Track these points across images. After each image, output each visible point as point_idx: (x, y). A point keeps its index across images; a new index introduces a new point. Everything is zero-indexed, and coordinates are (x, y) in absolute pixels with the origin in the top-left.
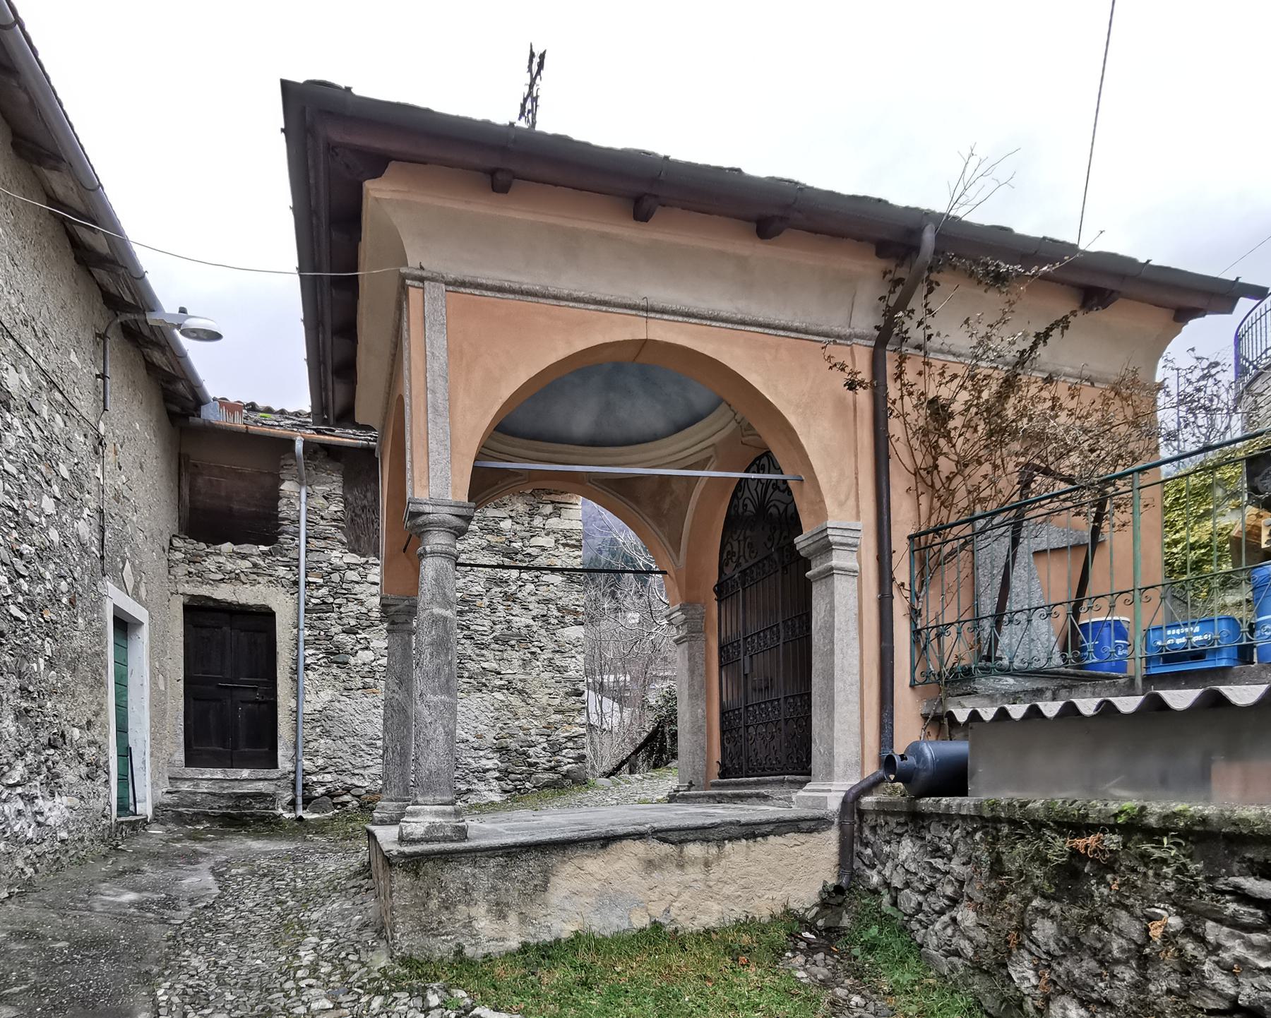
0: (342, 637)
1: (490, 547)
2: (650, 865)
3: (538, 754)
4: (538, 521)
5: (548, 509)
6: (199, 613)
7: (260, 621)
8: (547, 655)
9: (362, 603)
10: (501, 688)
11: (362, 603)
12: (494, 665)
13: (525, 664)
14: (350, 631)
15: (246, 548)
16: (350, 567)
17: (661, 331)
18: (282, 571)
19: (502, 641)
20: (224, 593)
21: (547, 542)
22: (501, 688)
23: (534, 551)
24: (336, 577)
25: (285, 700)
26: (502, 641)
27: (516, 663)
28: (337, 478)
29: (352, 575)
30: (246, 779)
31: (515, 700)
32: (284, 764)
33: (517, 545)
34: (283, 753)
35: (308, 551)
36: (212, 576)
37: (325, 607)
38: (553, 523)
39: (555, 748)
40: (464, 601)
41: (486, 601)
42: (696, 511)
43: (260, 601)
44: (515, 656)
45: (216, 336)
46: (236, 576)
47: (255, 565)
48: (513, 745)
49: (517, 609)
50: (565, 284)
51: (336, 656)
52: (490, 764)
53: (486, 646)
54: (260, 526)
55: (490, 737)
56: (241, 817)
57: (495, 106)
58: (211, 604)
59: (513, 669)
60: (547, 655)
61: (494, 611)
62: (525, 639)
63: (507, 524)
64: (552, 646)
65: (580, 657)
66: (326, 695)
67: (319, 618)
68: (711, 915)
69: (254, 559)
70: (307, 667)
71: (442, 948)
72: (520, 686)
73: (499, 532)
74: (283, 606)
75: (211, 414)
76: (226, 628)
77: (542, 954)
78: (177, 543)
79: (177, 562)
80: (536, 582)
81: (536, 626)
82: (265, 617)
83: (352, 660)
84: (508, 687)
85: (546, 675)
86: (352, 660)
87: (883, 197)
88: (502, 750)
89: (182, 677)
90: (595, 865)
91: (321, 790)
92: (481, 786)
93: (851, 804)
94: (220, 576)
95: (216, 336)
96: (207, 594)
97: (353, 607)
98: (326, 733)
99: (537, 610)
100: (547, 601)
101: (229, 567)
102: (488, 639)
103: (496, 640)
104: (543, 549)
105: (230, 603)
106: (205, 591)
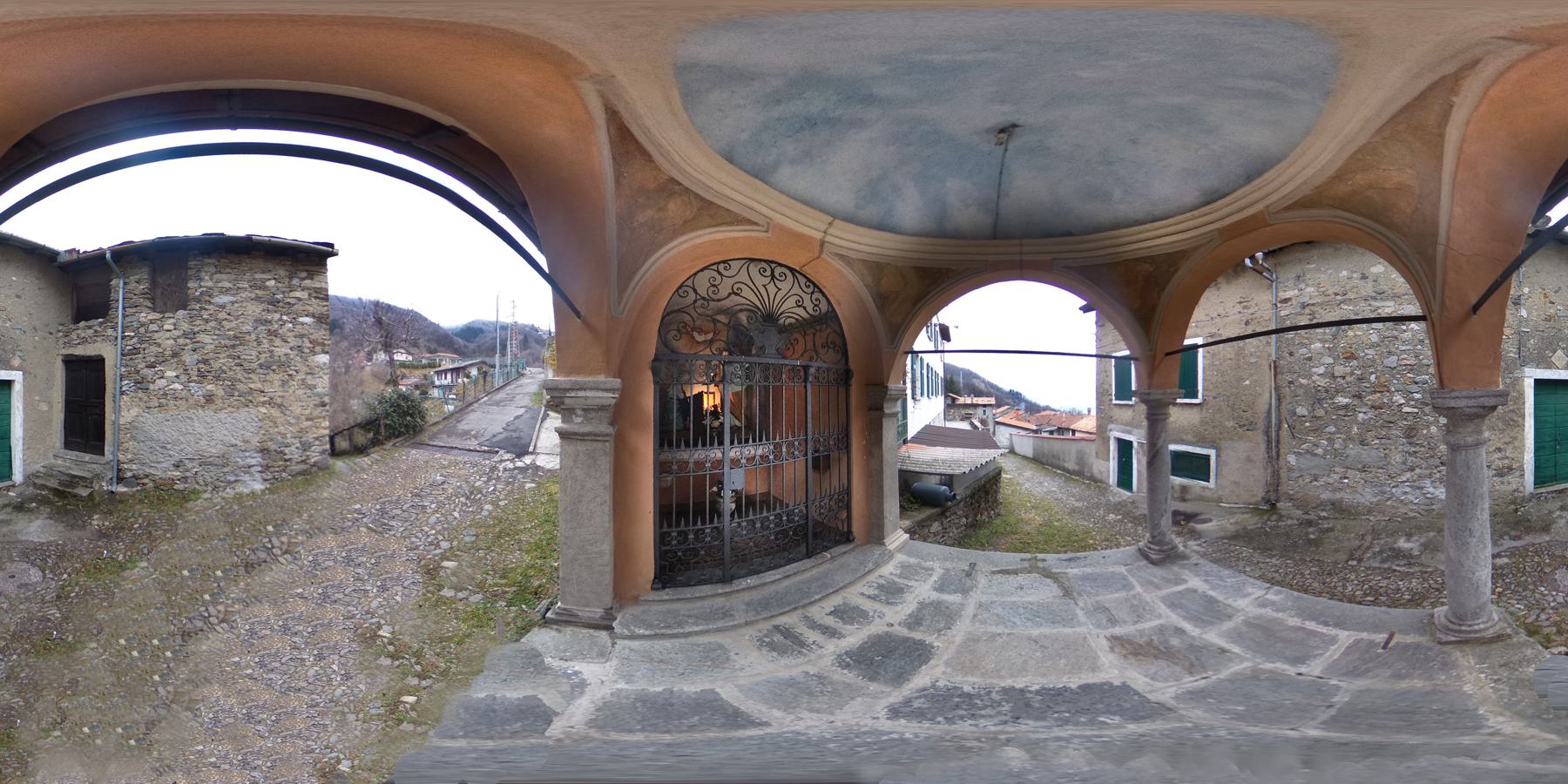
0: (146, 371)
1: (258, 298)
3: (293, 452)
4: (295, 282)
5: (304, 275)
6: (71, 363)
7: (99, 362)
8: (301, 376)
9: (159, 345)
10: (264, 403)
11: (159, 345)
12: (259, 386)
13: (284, 383)
14: (151, 366)
15: (91, 323)
16: (152, 322)
18: (110, 332)
19: (266, 366)
21: (303, 295)
22: (264, 403)
23: (292, 301)
24: (142, 330)
25: (109, 416)
26: (266, 366)
27: (277, 383)
28: (145, 270)
29: (153, 327)
31: (275, 412)
32: (108, 455)
33: (279, 296)
34: (108, 448)
35: (124, 316)
37: (135, 351)
38: (308, 282)
39: (306, 447)
40: (236, 337)
41: (253, 336)
44: (276, 378)
48: (273, 446)
49: (278, 342)
51: (141, 384)
52: (254, 462)
53: (254, 371)
55: (255, 442)
59: (274, 389)
60: (301, 376)
61: (259, 343)
62: (283, 365)
63: (272, 283)
64: (305, 369)
65: (326, 378)
66: (134, 412)
70: (122, 393)
72: (279, 401)
73: (265, 288)
74: (110, 353)
80: (294, 321)
81: (292, 354)
82: (99, 362)
83: (152, 387)
84: (270, 402)
85: (300, 392)
86: (152, 387)
87: (400, 299)
88: (264, 451)
91: (129, 474)
92: (246, 478)
97: (154, 349)
98: (133, 438)
99: (293, 342)
100: (302, 336)
102: (254, 366)
103: (261, 366)
104: (299, 299)
106: (70, 351)
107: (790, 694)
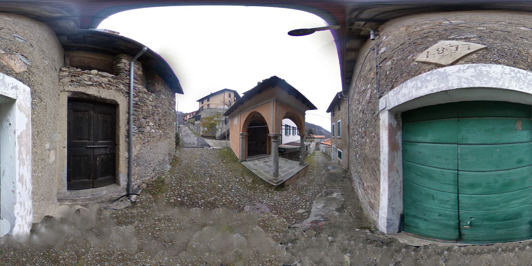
6: (77, 102)
15: (105, 74)
18: (121, 87)
20: (92, 91)
36: (86, 82)
42: (377, 146)
43: (112, 98)
45: (293, 33)
47: (109, 81)
58: (85, 96)
67: (21, 180)
69: (109, 79)
76: (92, 112)
78: (64, 69)
79: (64, 77)
89: (66, 146)
94: (90, 83)
95: (293, 33)
96: (83, 91)
101: (95, 79)
105: (96, 97)
107: (260, 163)
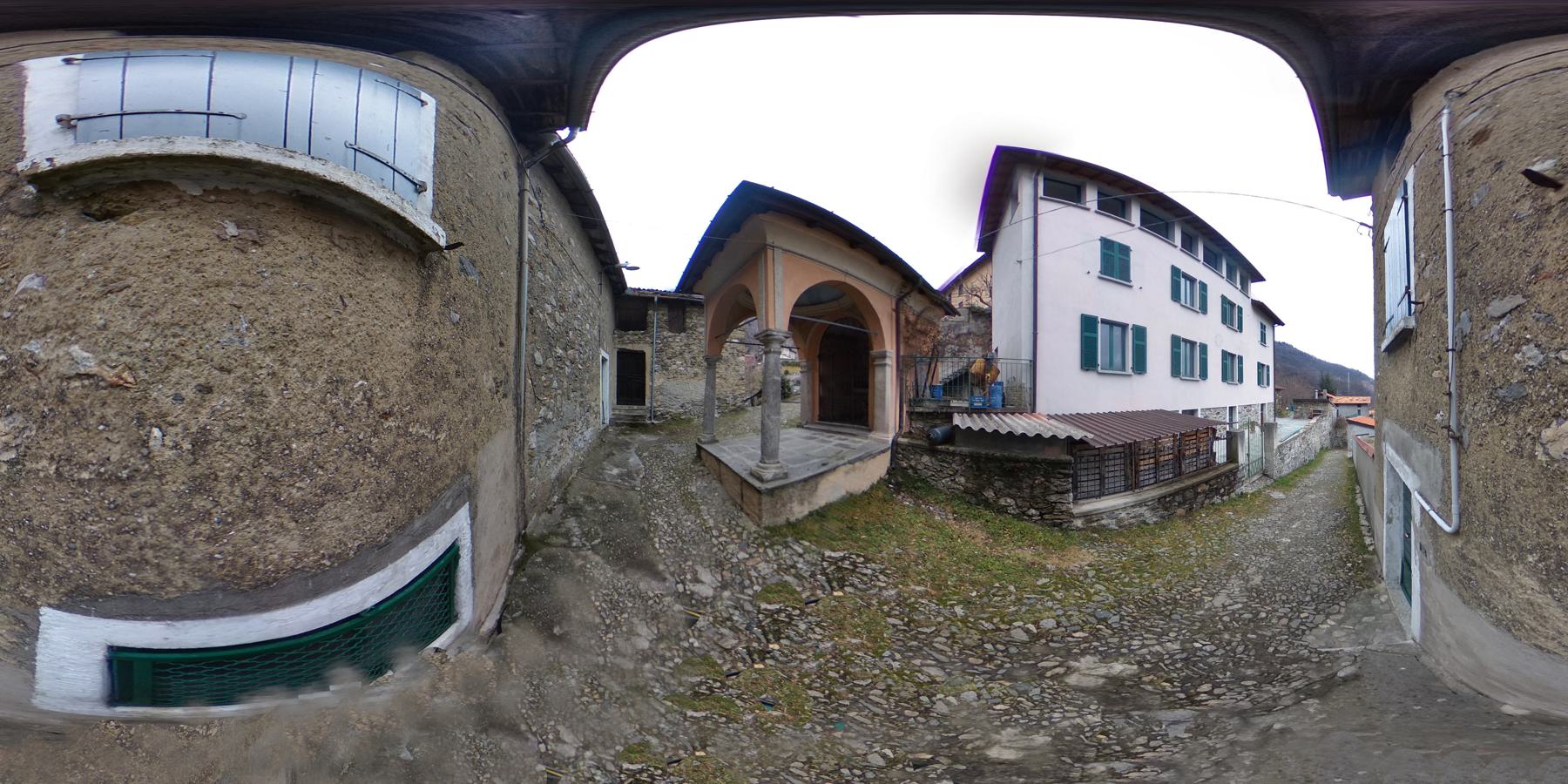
2: (847, 473)
3: (730, 400)
17: (849, 281)
20: (629, 347)
30: (636, 410)
32: (648, 404)
39: (735, 398)
46: (635, 342)
50: (822, 259)
51: (665, 367)
54: (641, 324)
56: (636, 425)
57: (623, 257)
68: (865, 486)
71: (781, 520)
74: (648, 350)
75: (628, 292)
77: (820, 515)
82: (643, 354)
90: (831, 478)
93: (895, 443)
